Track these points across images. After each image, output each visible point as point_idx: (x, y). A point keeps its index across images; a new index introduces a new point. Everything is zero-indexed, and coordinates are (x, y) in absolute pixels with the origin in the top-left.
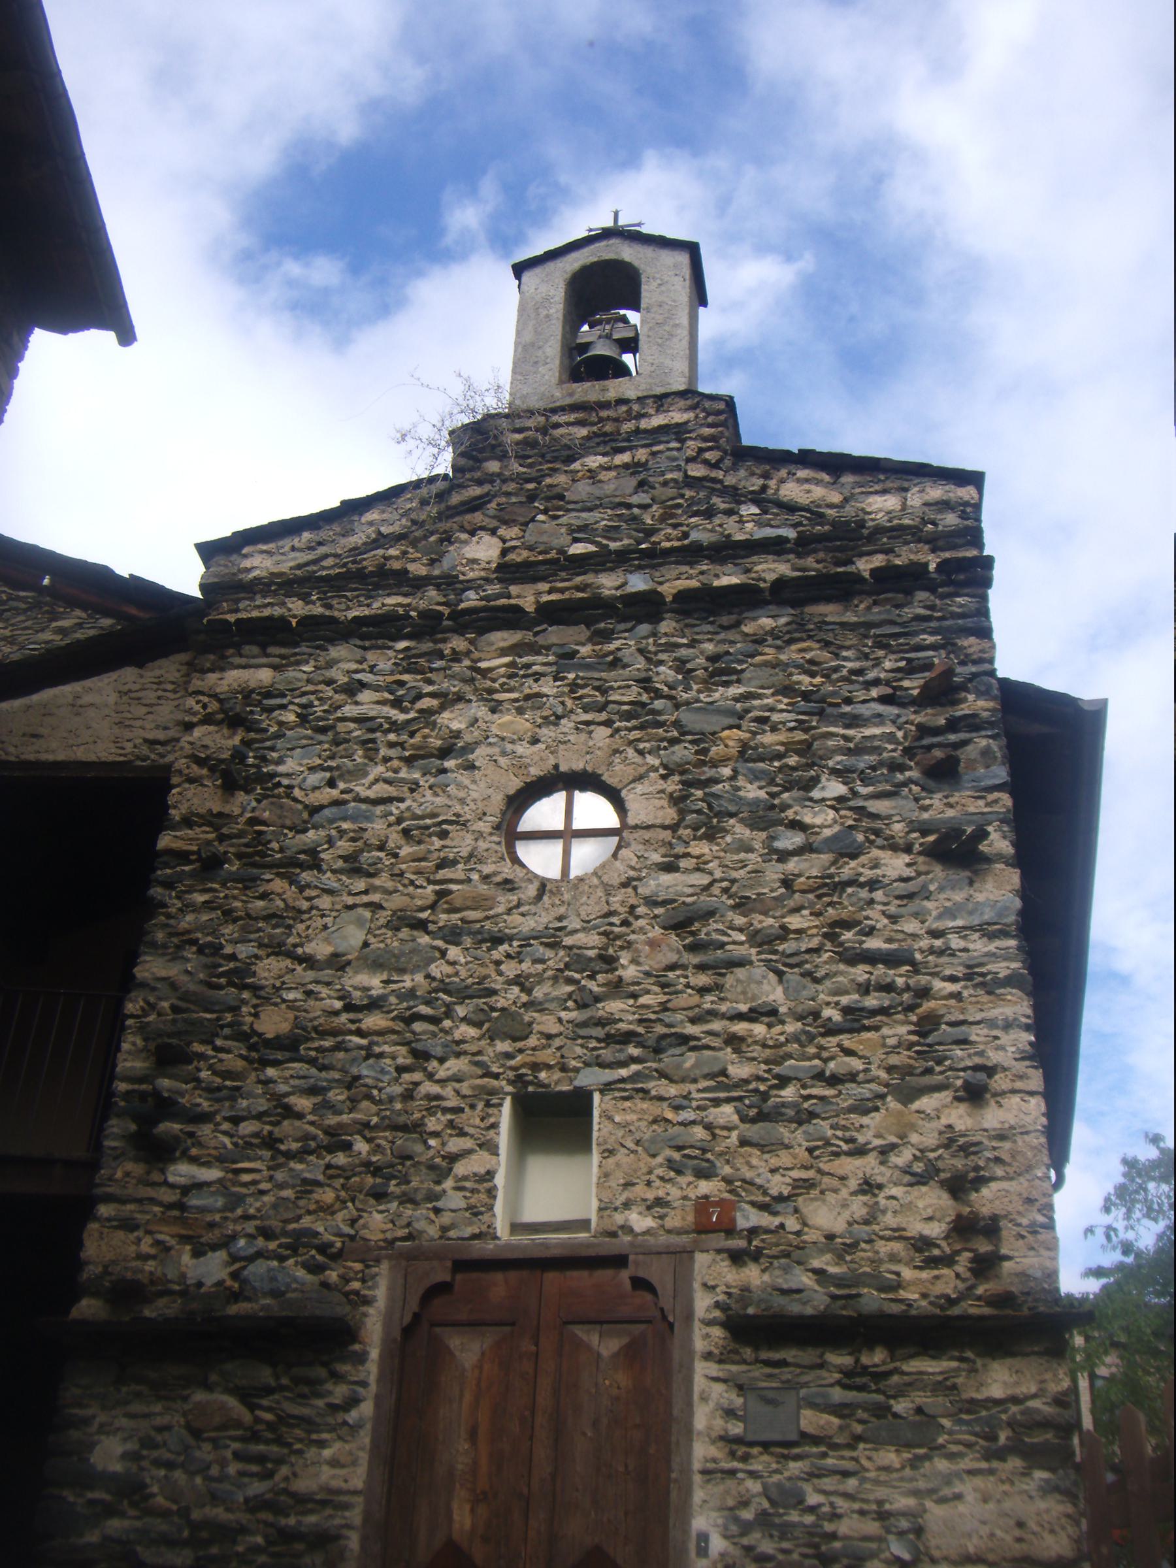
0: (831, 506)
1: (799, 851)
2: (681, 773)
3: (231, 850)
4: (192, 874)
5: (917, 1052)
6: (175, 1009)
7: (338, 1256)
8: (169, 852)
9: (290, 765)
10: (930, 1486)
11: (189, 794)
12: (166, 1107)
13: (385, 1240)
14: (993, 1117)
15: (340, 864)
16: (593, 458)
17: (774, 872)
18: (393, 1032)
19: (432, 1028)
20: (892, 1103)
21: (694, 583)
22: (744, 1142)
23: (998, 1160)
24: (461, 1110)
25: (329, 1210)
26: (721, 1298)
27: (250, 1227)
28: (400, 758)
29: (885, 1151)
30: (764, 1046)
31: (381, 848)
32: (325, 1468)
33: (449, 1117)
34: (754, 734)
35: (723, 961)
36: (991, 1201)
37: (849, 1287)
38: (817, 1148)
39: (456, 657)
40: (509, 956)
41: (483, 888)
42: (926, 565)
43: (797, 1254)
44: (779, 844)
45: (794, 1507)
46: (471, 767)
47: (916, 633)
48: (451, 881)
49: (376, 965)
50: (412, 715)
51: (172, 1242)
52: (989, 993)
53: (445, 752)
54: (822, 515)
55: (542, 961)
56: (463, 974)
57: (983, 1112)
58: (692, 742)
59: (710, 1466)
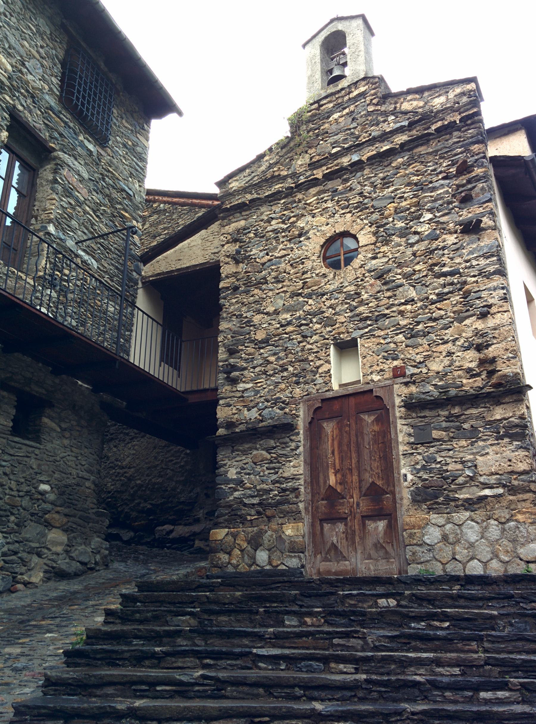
1: (417, 242)
4: (231, 294)
6: (232, 337)
8: (223, 288)
9: (254, 251)
12: (234, 368)
14: (491, 322)
15: (273, 280)
17: (409, 251)
20: (456, 324)
22: (407, 346)
23: (494, 337)
24: (319, 352)
26: (403, 398)
27: (262, 399)
29: (454, 341)
30: (411, 312)
31: (285, 272)
34: (399, 203)
39: (300, 201)
42: (455, 121)
44: (410, 241)
46: (309, 238)
47: (455, 149)
48: (307, 278)
50: (289, 225)
51: (241, 408)
53: (300, 235)
56: (314, 308)
58: (378, 212)
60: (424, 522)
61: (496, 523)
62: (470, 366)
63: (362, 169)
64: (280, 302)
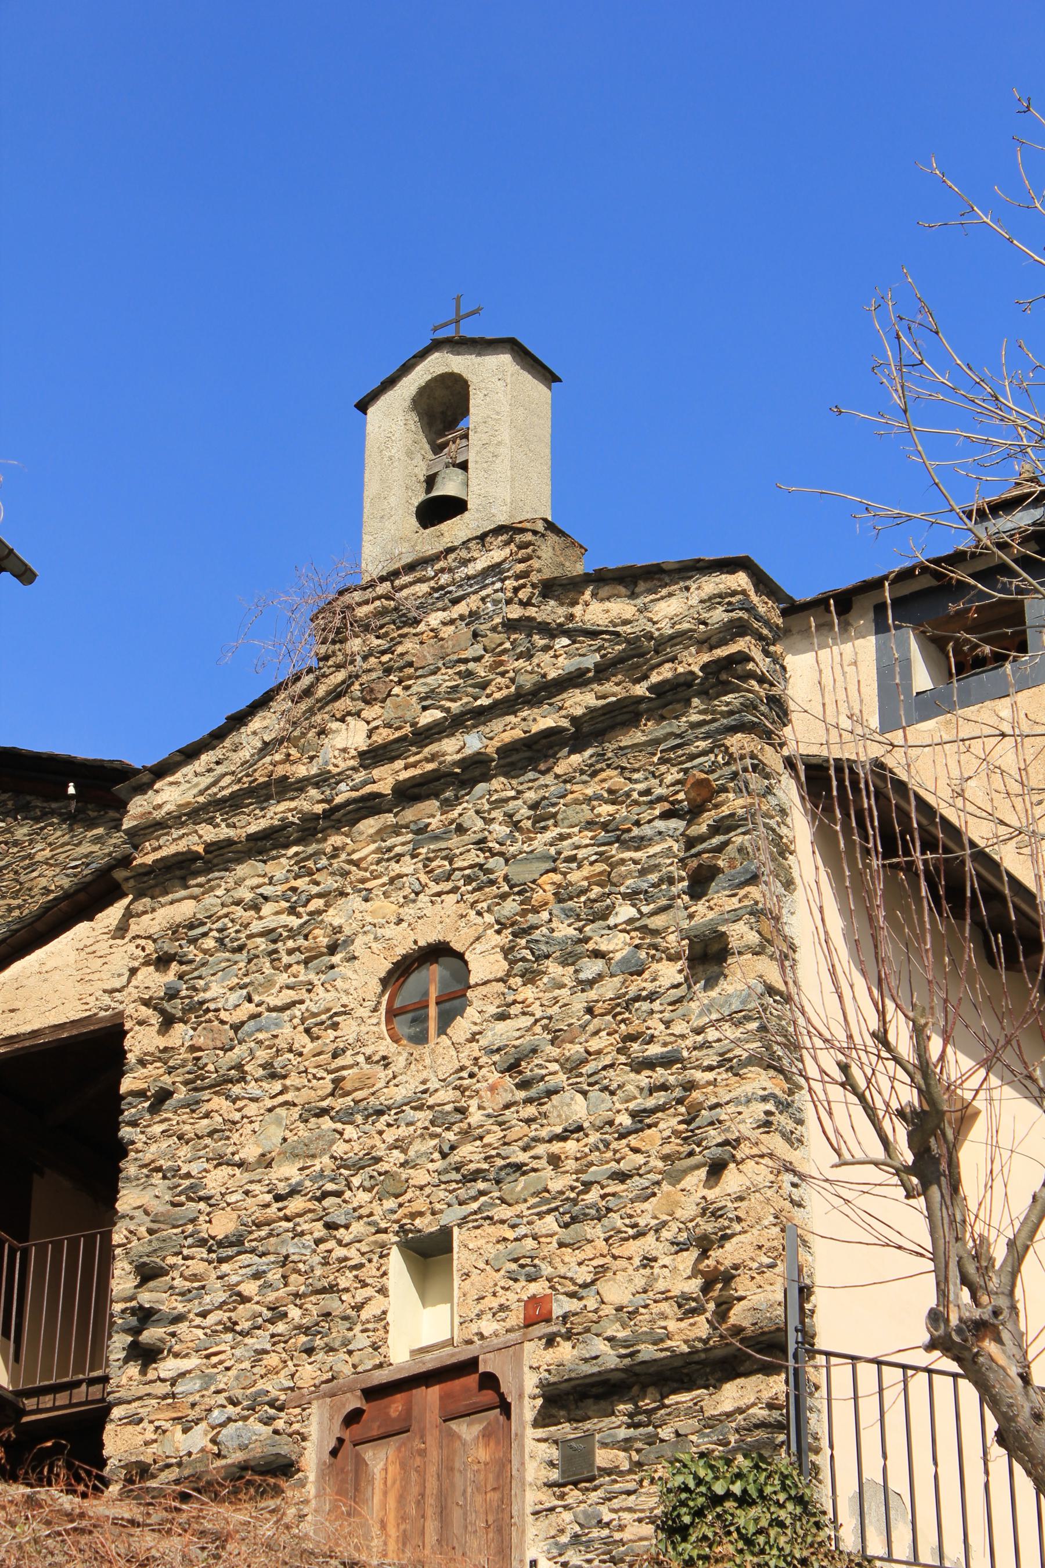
3: (177, 1079)
9: (215, 990)
11: (139, 1037)
13: (315, 1386)
16: (434, 615)
17: (579, 1002)
18: (310, 1211)
19: (338, 1200)
20: (666, 1187)
21: (518, 734)
24: (362, 1265)
27: (221, 1399)
33: (355, 1273)
38: (611, 1237)
40: (389, 1125)
43: (595, 1328)
48: (344, 1068)
50: (305, 918)
52: (736, 1075)
54: (617, 634)
59: (539, 1507)
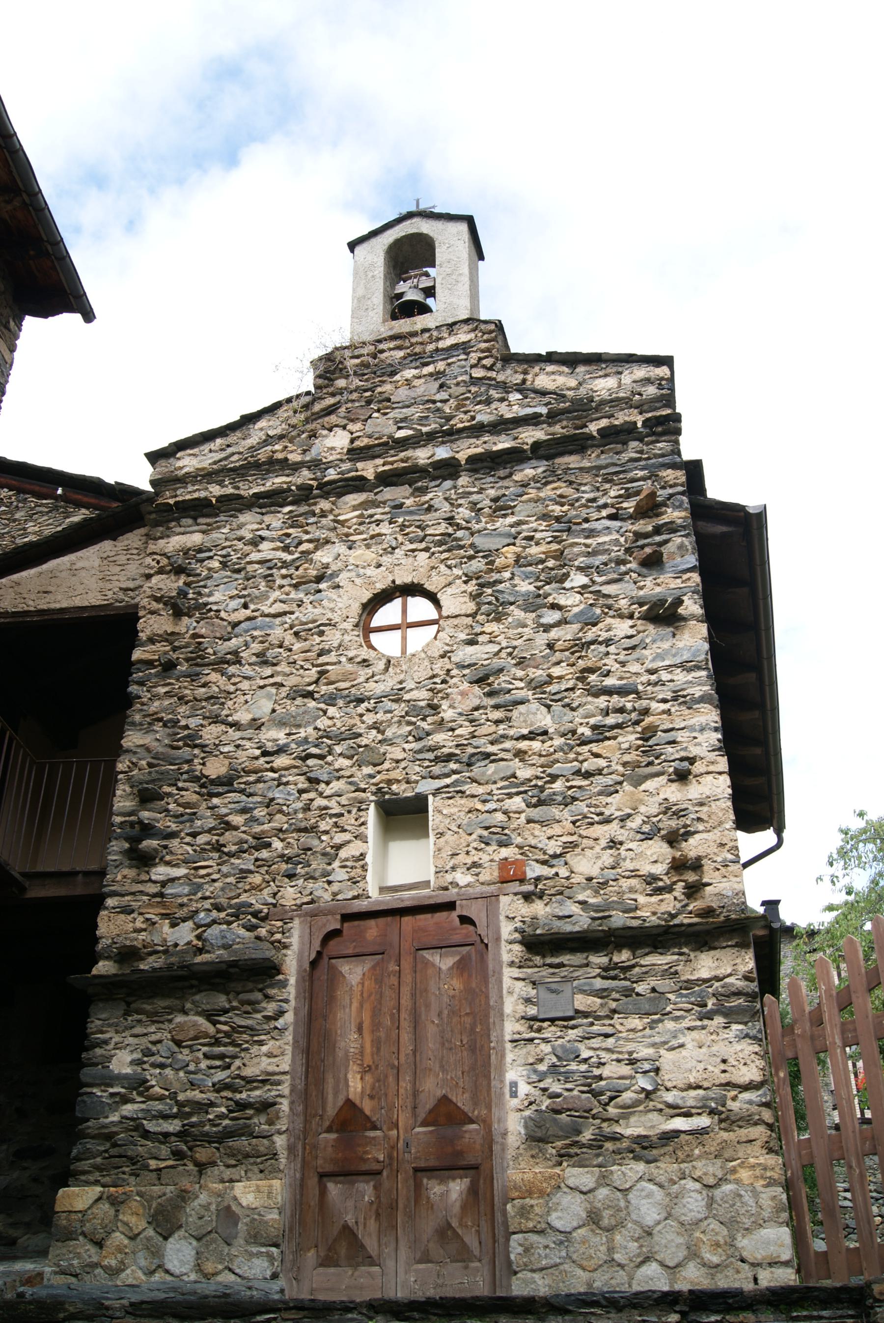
0: (569, 389)
1: (558, 624)
2: (477, 579)
4: (156, 675)
5: (643, 752)
6: (150, 765)
7: (264, 919)
8: (140, 661)
9: (217, 597)
10: (663, 1039)
11: (151, 622)
12: (147, 830)
14: (695, 790)
15: (254, 659)
17: (542, 639)
20: (627, 786)
22: (529, 821)
24: (342, 815)
25: (257, 888)
26: (519, 925)
27: (207, 904)
28: (290, 585)
30: (540, 756)
31: (281, 647)
32: (264, 1058)
34: (525, 548)
35: (510, 701)
36: (696, 847)
37: (603, 911)
38: (578, 820)
39: (323, 514)
41: (349, 667)
42: (635, 423)
43: (567, 892)
44: (544, 621)
45: (573, 1060)
46: (338, 587)
47: (631, 470)
48: (327, 664)
49: (282, 724)
50: (297, 555)
52: (689, 708)
53: (319, 579)
55: (390, 712)
56: (339, 725)
57: (686, 785)
58: (483, 557)
59: (517, 1037)
60: (553, 1182)
61: (698, 1186)
62: (653, 871)
63: (454, 476)
64: (267, 706)
